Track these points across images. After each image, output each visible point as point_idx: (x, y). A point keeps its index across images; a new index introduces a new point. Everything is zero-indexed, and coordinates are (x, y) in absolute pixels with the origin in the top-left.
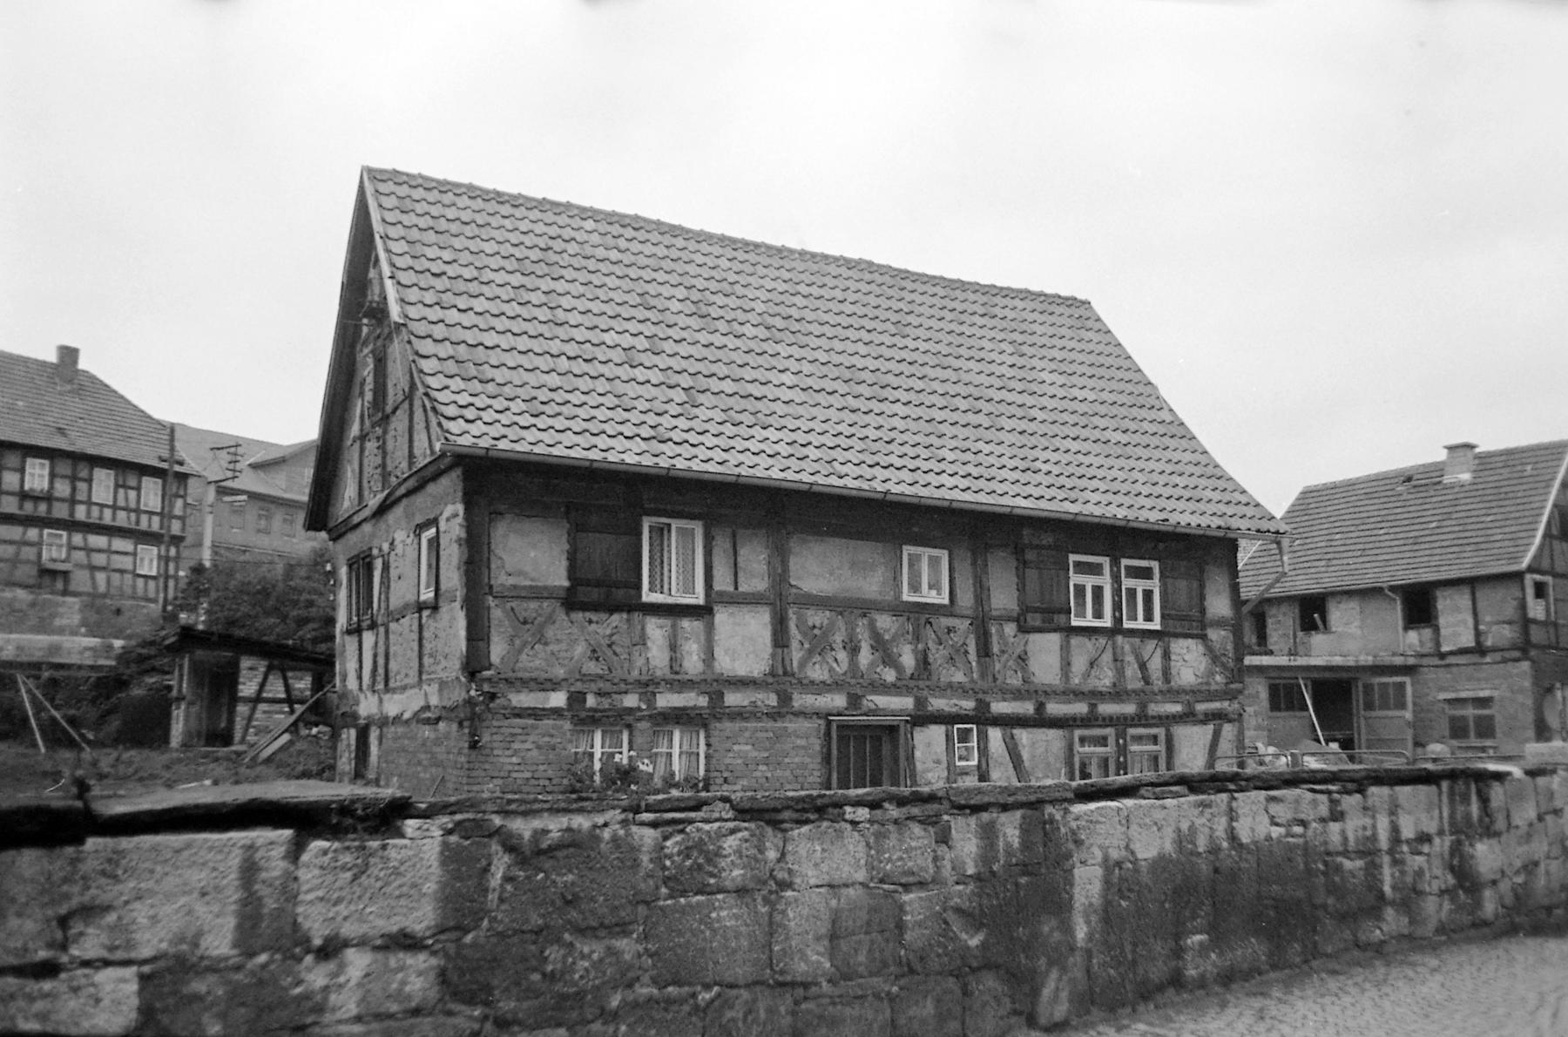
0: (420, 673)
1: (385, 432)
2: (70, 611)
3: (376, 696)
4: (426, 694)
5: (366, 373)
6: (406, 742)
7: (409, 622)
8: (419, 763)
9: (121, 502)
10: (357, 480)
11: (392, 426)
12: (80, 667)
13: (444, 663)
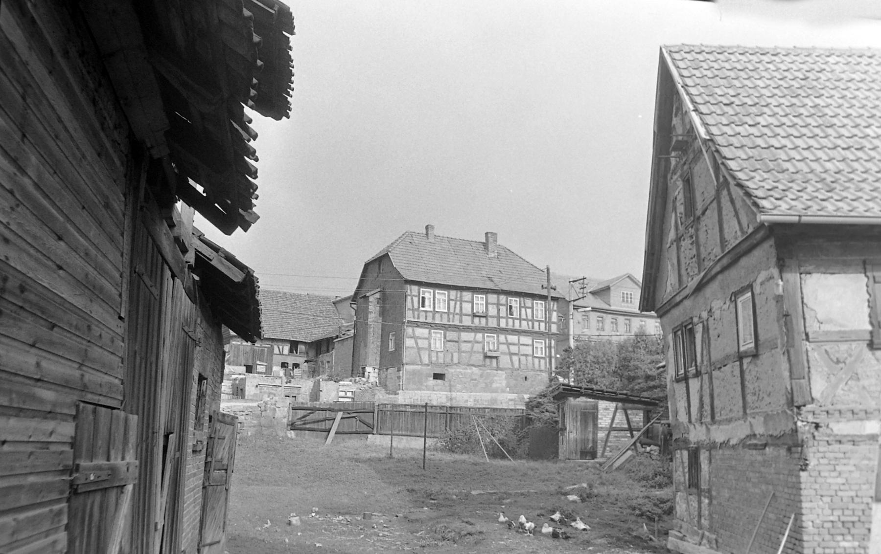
0: (745, 407)
1: (697, 230)
2: (500, 379)
3: (704, 427)
4: (751, 425)
5: (677, 193)
6: (734, 463)
7: (733, 368)
8: (748, 480)
9: (524, 316)
10: (677, 272)
11: (703, 224)
12: (505, 410)
13: (767, 400)
